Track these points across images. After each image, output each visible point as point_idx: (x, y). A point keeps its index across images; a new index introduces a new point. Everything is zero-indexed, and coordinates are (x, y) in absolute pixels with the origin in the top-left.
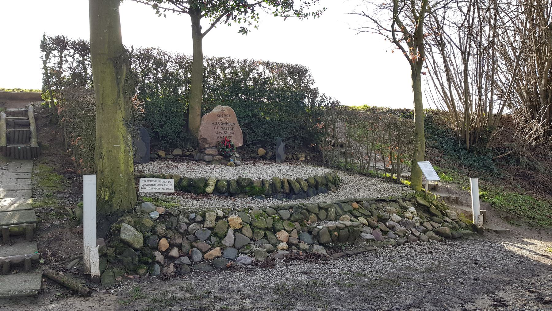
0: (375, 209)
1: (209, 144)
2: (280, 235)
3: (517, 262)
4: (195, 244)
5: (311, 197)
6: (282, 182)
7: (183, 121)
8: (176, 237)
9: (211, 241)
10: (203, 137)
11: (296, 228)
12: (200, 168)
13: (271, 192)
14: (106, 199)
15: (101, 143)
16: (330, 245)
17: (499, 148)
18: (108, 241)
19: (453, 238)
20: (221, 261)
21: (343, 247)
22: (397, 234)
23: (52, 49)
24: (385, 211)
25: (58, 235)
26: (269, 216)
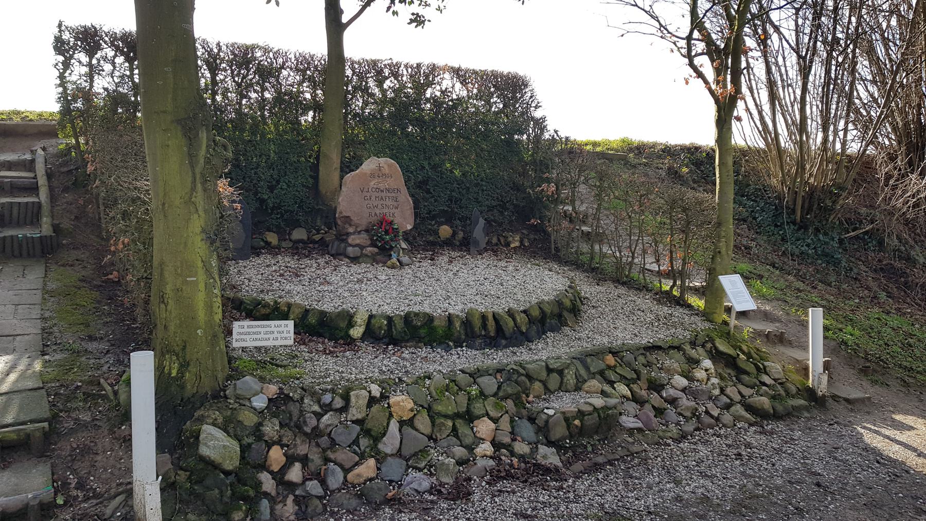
0: (643, 365)
1: (354, 227)
2: (480, 426)
3: (888, 479)
4: (332, 456)
5: (532, 342)
6: (484, 317)
7: (309, 179)
8: (298, 441)
9: (359, 446)
10: (345, 214)
11: (507, 412)
13: (463, 337)
14: (172, 375)
15: (161, 274)
16: (567, 443)
17: (850, 219)
18: (177, 456)
19: (776, 416)
20: (376, 488)
21: (589, 445)
22: (680, 414)
23: (74, 48)
24: (661, 369)
25: (87, 442)
26: (460, 389)
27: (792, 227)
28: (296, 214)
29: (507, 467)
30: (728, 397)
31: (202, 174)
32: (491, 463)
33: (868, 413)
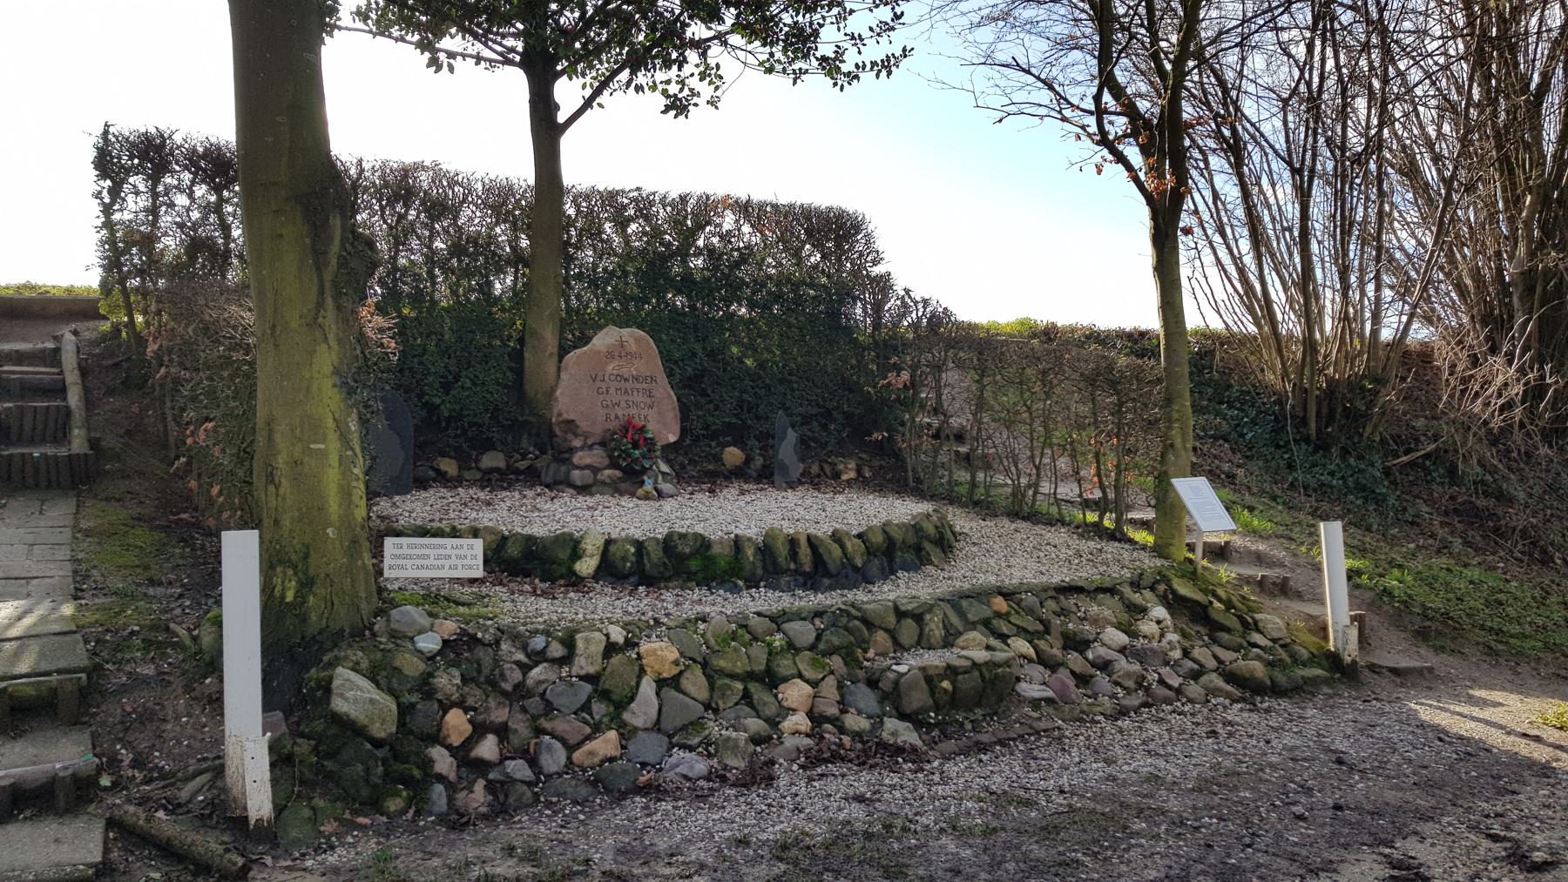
2: (789, 692)
4: (547, 725)
6: (793, 542)
7: (508, 373)
8: (492, 704)
9: (591, 714)
10: (565, 416)
11: (832, 673)
19: (1276, 691)
24: (1084, 619)
26: (755, 639)
27: (1304, 446)
28: (488, 429)
29: (833, 747)
30: (1195, 661)
31: (335, 283)
32: (808, 741)
33: (1430, 688)
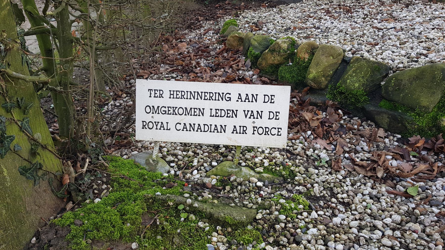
12: (413, 14)
